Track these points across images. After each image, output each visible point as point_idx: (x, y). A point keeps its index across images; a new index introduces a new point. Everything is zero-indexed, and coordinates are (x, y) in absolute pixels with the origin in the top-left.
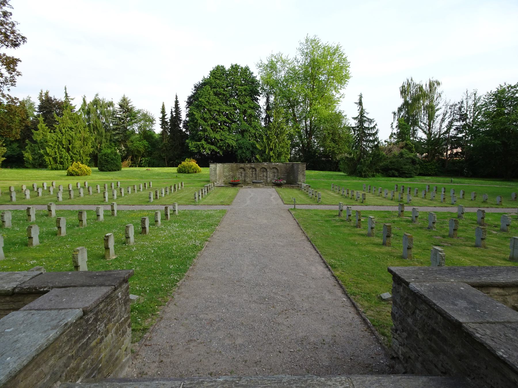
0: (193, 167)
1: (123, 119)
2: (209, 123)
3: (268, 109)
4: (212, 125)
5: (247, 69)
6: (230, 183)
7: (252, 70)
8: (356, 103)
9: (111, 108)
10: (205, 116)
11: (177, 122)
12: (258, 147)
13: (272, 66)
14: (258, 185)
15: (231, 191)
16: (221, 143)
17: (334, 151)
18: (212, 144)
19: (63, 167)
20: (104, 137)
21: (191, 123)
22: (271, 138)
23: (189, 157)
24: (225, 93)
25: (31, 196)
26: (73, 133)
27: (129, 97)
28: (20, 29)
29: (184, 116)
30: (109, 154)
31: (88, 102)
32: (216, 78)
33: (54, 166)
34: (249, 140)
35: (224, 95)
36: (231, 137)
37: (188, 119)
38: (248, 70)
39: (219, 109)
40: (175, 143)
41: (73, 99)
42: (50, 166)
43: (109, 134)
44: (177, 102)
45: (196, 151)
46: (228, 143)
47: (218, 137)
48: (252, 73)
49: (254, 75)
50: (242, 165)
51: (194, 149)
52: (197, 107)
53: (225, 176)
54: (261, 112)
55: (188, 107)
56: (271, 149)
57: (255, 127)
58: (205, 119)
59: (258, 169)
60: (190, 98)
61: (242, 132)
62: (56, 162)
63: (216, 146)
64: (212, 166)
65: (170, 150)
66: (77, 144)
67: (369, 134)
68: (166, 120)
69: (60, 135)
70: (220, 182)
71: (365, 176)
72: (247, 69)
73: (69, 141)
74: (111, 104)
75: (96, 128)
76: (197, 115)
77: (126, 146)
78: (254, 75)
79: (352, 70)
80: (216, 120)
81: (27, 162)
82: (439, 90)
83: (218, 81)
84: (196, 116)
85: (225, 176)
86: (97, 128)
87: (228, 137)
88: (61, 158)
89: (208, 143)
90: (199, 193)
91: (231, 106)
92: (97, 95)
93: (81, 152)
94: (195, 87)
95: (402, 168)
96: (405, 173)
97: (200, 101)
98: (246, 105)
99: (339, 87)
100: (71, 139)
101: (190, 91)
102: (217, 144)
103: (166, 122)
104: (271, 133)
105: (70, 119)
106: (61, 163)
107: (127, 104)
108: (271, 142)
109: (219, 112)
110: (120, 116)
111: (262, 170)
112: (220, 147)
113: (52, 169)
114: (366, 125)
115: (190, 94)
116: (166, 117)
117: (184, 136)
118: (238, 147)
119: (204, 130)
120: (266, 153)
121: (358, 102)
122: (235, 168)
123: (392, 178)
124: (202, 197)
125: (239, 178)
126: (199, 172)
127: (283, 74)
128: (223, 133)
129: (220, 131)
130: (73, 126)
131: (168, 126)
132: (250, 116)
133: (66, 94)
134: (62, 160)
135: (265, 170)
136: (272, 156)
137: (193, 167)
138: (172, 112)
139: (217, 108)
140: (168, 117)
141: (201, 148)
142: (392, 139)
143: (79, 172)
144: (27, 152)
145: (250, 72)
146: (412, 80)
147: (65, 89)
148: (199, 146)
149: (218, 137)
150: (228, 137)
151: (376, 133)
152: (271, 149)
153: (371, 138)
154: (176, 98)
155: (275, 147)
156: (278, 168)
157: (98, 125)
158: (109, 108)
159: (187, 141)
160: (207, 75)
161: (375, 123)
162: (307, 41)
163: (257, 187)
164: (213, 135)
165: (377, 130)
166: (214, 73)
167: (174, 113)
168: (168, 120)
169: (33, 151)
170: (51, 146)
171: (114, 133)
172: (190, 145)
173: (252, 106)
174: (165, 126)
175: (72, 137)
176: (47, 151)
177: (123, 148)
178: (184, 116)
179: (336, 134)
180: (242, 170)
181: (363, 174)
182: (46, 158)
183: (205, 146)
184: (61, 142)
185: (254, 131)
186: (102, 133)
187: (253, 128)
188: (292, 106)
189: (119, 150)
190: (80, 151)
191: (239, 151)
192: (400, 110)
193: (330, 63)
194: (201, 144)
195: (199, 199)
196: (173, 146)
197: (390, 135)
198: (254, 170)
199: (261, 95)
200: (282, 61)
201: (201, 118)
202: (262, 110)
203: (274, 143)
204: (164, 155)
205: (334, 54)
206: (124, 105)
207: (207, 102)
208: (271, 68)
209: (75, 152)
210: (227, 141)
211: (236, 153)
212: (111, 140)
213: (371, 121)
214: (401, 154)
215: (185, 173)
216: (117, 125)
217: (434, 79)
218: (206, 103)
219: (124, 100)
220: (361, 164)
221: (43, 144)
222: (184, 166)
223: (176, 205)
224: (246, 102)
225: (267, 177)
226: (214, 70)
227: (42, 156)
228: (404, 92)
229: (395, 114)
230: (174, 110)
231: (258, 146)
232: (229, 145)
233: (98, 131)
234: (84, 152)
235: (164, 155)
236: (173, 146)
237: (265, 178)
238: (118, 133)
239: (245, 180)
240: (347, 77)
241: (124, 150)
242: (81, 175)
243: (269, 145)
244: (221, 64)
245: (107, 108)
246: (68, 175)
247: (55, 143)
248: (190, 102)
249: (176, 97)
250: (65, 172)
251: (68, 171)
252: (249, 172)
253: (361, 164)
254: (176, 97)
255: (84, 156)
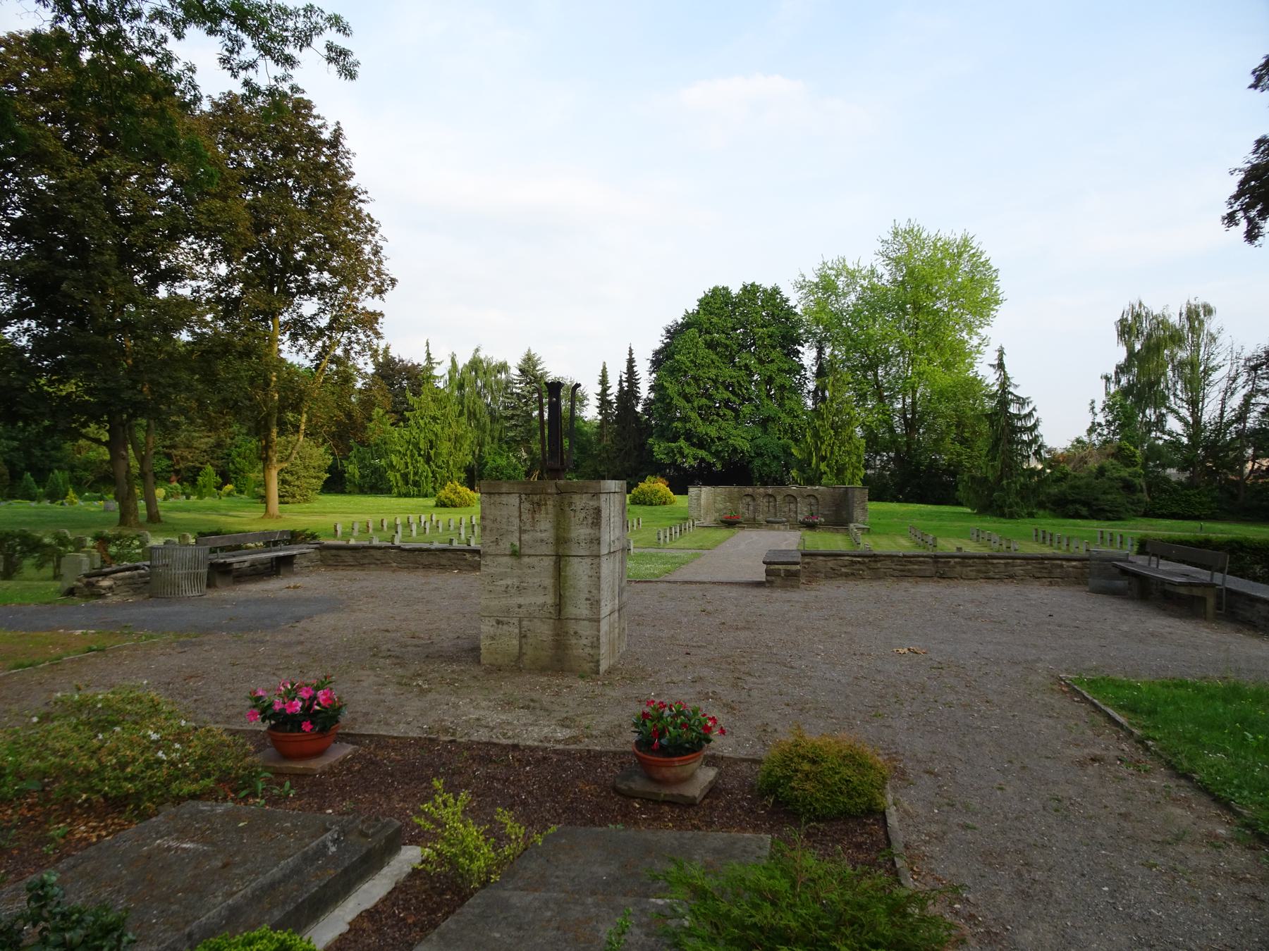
0: (660, 494)
1: (524, 397)
2: (695, 404)
3: (820, 373)
4: (700, 408)
5: (776, 291)
6: (722, 522)
7: (785, 294)
8: (991, 365)
9: (503, 376)
10: (687, 390)
11: (630, 401)
12: (795, 453)
13: (826, 286)
14: (776, 526)
15: (724, 533)
16: (718, 446)
17: (960, 462)
18: (701, 445)
19: (419, 491)
20: (488, 432)
21: (659, 405)
22: (821, 434)
23: (653, 474)
24: (728, 342)
25: (418, 534)
26: (437, 428)
27: (538, 352)
28: (389, 268)
29: (644, 391)
30: (504, 467)
31: (460, 366)
32: (711, 314)
33: (403, 490)
34: (773, 440)
35: (726, 346)
36: (740, 432)
37: (652, 396)
38: (778, 293)
39: (717, 376)
40: (626, 446)
41: (439, 363)
42: (396, 490)
43: (498, 427)
44: (631, 362)
45: (667, 461)
46: (733, 445)
47: (714, 434)
48: (787, 300)
49: (791, 303)
50: (749, 490)
51: (663, 457)
52: (672, 372)
53: (718, 511)
54: (807, 378)
55: (653, 372)
56: (823, 459)
57: (792, 410)
58: (687, 398)
59: (779, 498)
60: (657, 353)
61: (764, 423)
62: (407, 483)
63: (709, 450)
64: (693, 491)
65: (614, 458)
66: (445, 447)
67: (1020, 428)
68: (609, 398)
69: (415, 431)
70: (708, 521)
71: (1011, 516)
72: (776, 291)
73: (431, 442)
74: (503, 367)
75: (472, 415)
76: (672, 389)
77: (529, 451)
78: (791, 303)
79: (1004, 285)
80: (710, 397)
81: (350, 481)
82: (1211, 325)
83: (715, 320)
84: (669, 391)
85: (718, 511)
86: (475, 415)
87: (734, 432)
88: (416, 474)
89: (693, 445)
90: (665, 532)
91: (741, 369)
92: (477, 350)
93: (451, 463)
94: (668, 331)
95: (1097, 499)
96: (1103, 510)
97: (678, 361)
98: (773, 367)
99: (977, 323)
100: (434, 438)
101: (657, 341)
102: (710, 447)
103: (610, 403)
104: (824, 425)
105: (433, 401)
106: (416, 484)
107: (535, 367)
108: (822, 443)
109: (715, 381)
110: (519, 391)
111: (787, 499)
112: (717, 454)
113: (400, 495)
114: (1013, 409)
115: (658, 346)
116: (609, 392)
117: (646, 430)
118: (755, 453)
119: (685, 419)
120: (813, 466)
121: (996, 362)
122: (736, 495)
123: (1071, 521)
124: (671, 539)
125: (743, 513)
126: (671, 503)
127: (852, 298)
128: (724, 424)
129: (717, 421)
130: (438, 414)
131: (614, 410)
132: (782, 388)
133: (429, 354)
134: (417, 478)
135: (792, 498)
136: (825, 473)
137: (660, 494)
138: (621, 382)
139: (713, 373)
140: (614, 390)
141: (678, 456)
142: (1094, 436)
143: (457, 500)
144: (351, 463)
145: (781, 298)
146: (1140, 304)
147: (428, 345)
148: (673, 451)
149: (713, 431)
150: (734, 432)
151: (1035, 426)
152: (823, 459)
153: (1025, 437)
154: (631, 353)
155: (832, 453)
156: (819, 496)
157: (478, 411)
158: (499, 376)
159: (650, 441)
160: (693, 306)
161: (1031, 407)
162: (896, 234)
163: (774, 529)
164: (703, 429)
165: (1037, 420)
166: (707, 303)
167: (625, 384)
168: (612, 398)
169: (362, 460)
170: (400, 452)
171: (508, 425)
172: (656, 448)
173: (786, 367)
174: (606, 410)
175: (436, 435)
176: (392, 462)
177: (525, 455)
178: (644, 391)
179: (965, 426)
180: (749, 499)
181: (1006, 510)
182: (391, 475)
183: (686, 451)
184: (416, 445)
185: (789, 420)
186: (485, 424)
187: (787, 414)
188: (873, 366)
189: (516, 457)
190: (448, 461)
191: (757, 462)
192: (1121, 370)
193: (952, 273)
194: (677, 447)
195: (665, 541)
196: (621, 450)
197: (1088, 427)
198: (771, 499)
199: (807, 345)
200: (848, 273)
201: (679, 395)
202: (809, 374)
203: (829, 445)
204: (603, 468)
205: (960, 255)
206: (529, 367)
207: (692, 361)
208: (825, 289)
209: (440, 463)
210: (731, 442)
211: (751, 466)
212: (500, 439)
213: (1022, 402)
214: (1101, 471)
215: (645, 504)
216: (514, 408)
217: (1200, 302)
218: (689, 364)
219: (529, 359)
220: (1002, 489)
221: (381, 450)
222: (643, 490)
223: (632, 542)
224: (772, 361)
225: (796, 512)
226: (707, 295)
227: (376, 470)
228: (1126, 330)
229: (1107, 379)
230: (624, 377)
231: (795, 451)
232: (735, 450)
233: (478, 420)
234: (455, 464)
235: (603, 468)
236: (621, 450)
237: (792, 514)
238: (515, 425)
239: (754, 519)
240: (994, 300)
241: (525, 460)
242: (460, 505)
243: (818, 449)
244: (721, 285)
245: (496, 376)
246: (437, 506)
247: (406, 446)
248: (660, 360)
249: (631, 350)
250: (431, 502)
251: (439, 498)
252: (762, 502)
253: (1002, 489)
254: (631, 350)
255: (454, 470)
